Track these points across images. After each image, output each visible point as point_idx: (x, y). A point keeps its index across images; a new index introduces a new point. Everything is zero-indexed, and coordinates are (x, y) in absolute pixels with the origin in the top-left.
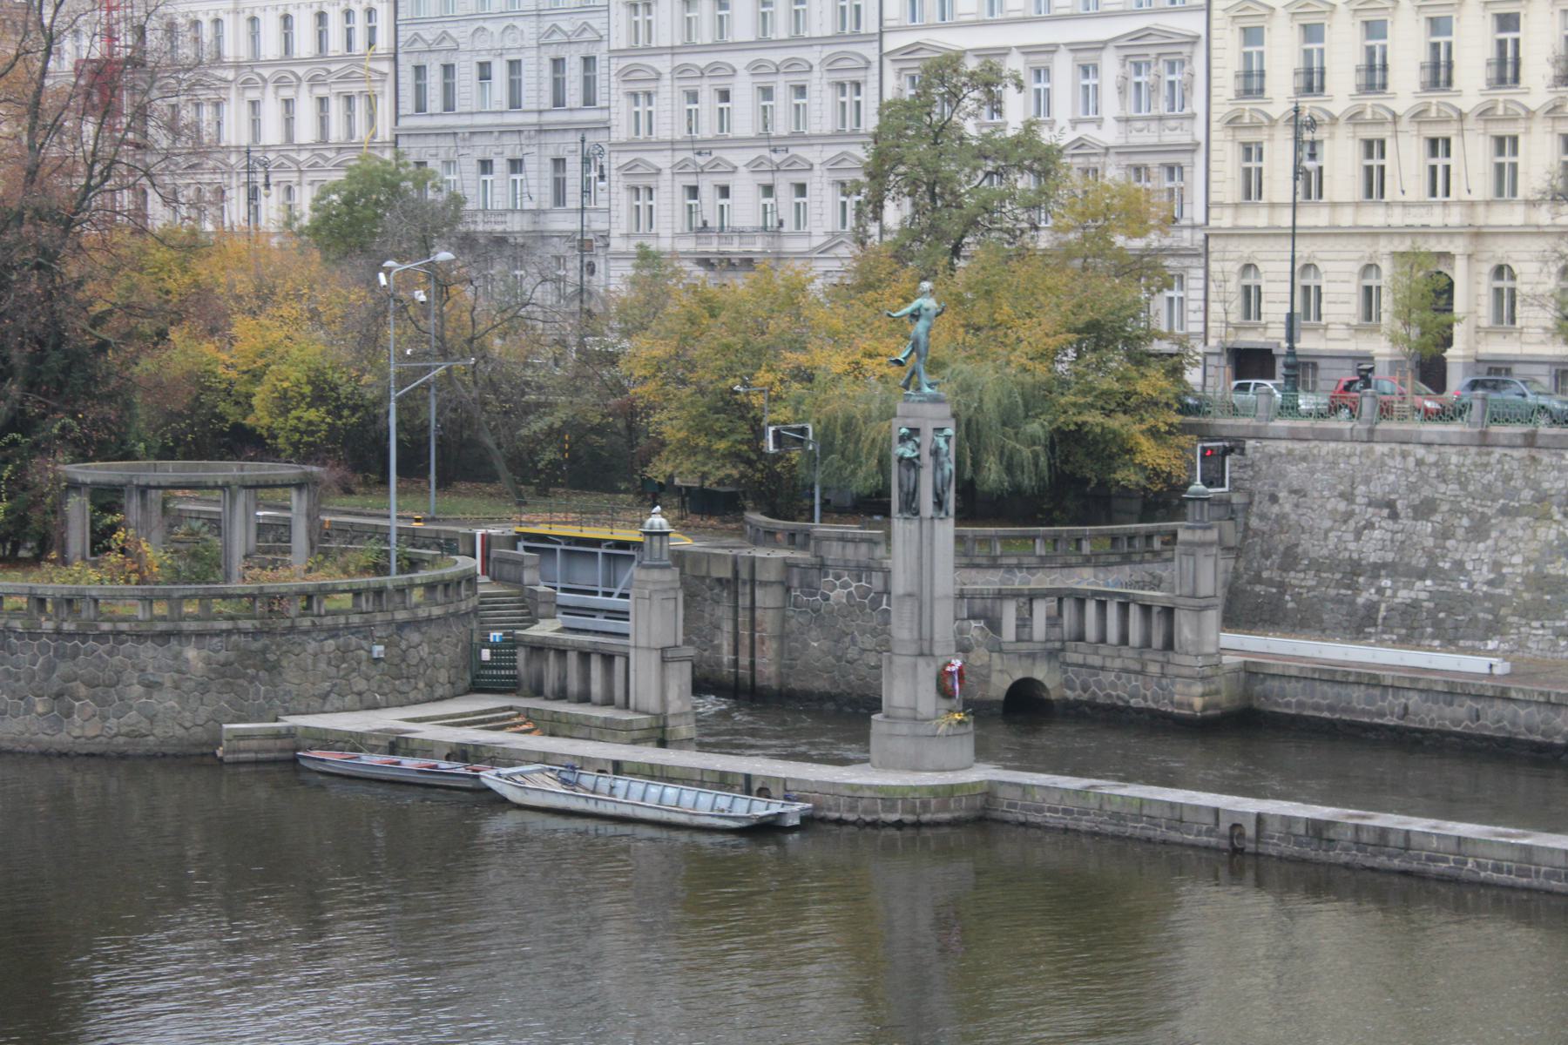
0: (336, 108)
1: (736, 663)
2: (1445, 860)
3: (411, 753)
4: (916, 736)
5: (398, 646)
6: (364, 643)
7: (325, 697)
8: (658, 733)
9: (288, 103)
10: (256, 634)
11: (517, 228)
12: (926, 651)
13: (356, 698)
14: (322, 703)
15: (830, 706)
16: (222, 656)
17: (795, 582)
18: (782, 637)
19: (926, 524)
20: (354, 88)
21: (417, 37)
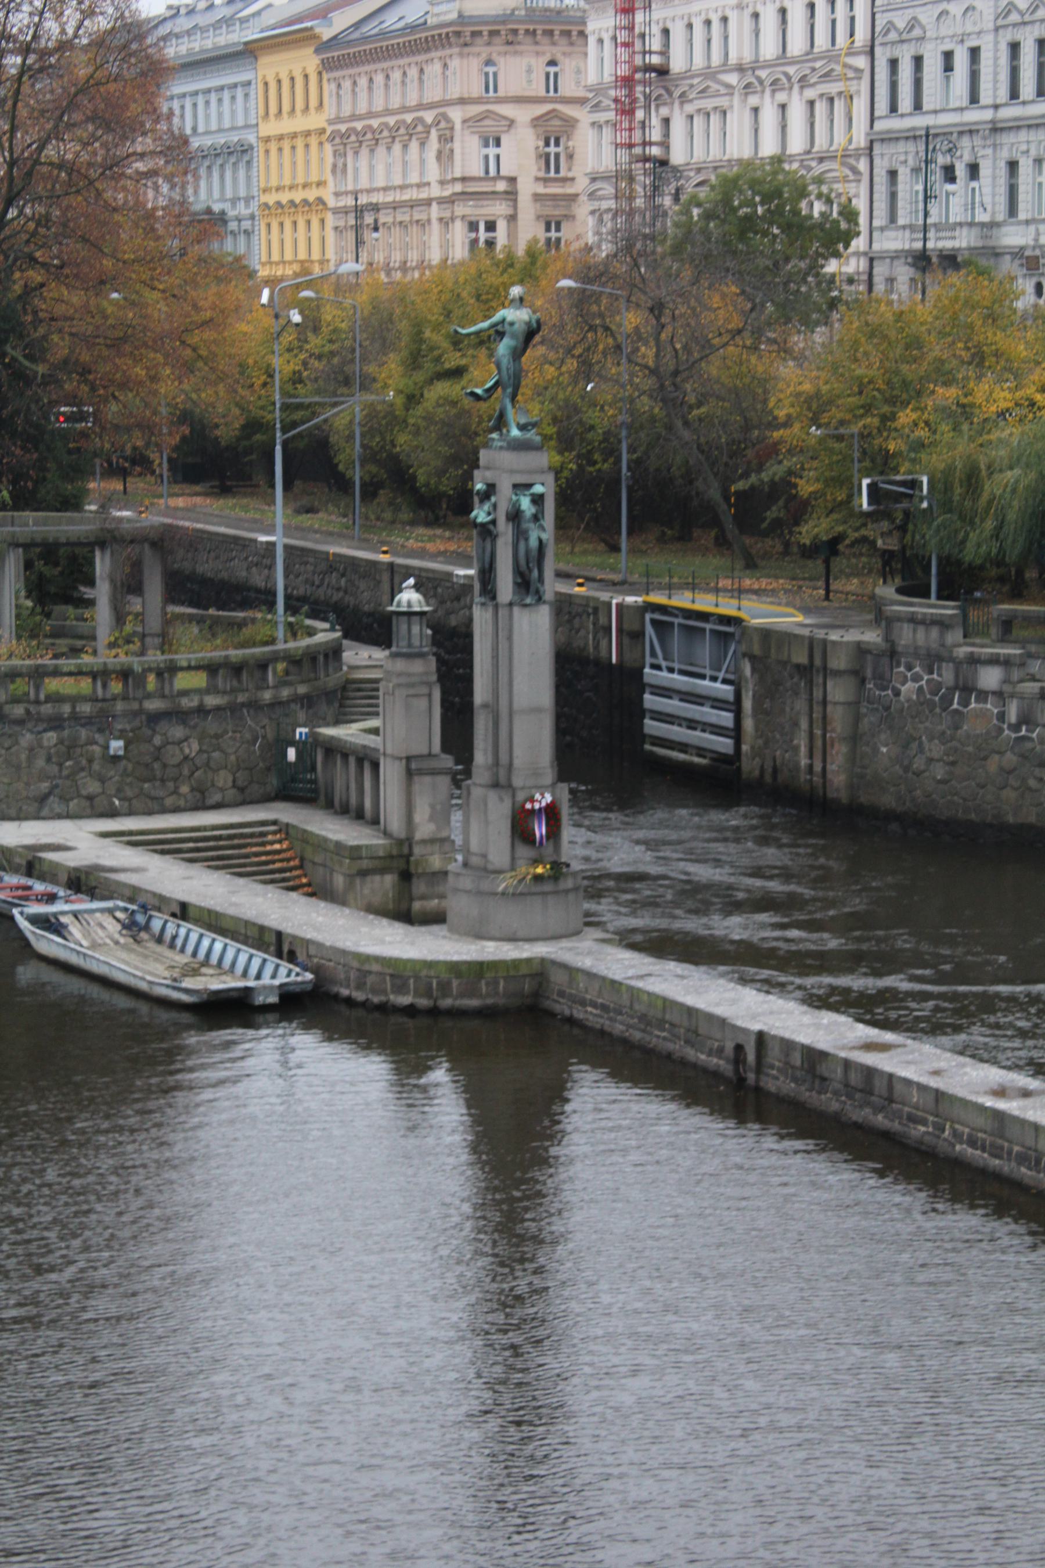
1: (811, 767)
3: (42, 878)
7: (43, 799)
9: (783, 107)
11: (964, 245)
12: (503, 780)
13: (86, 803)
15: (894, 827)
17: (869, 673)
18: (854, 738)
19: (502, 612)
20: (833, 88)
21: (890, 26)
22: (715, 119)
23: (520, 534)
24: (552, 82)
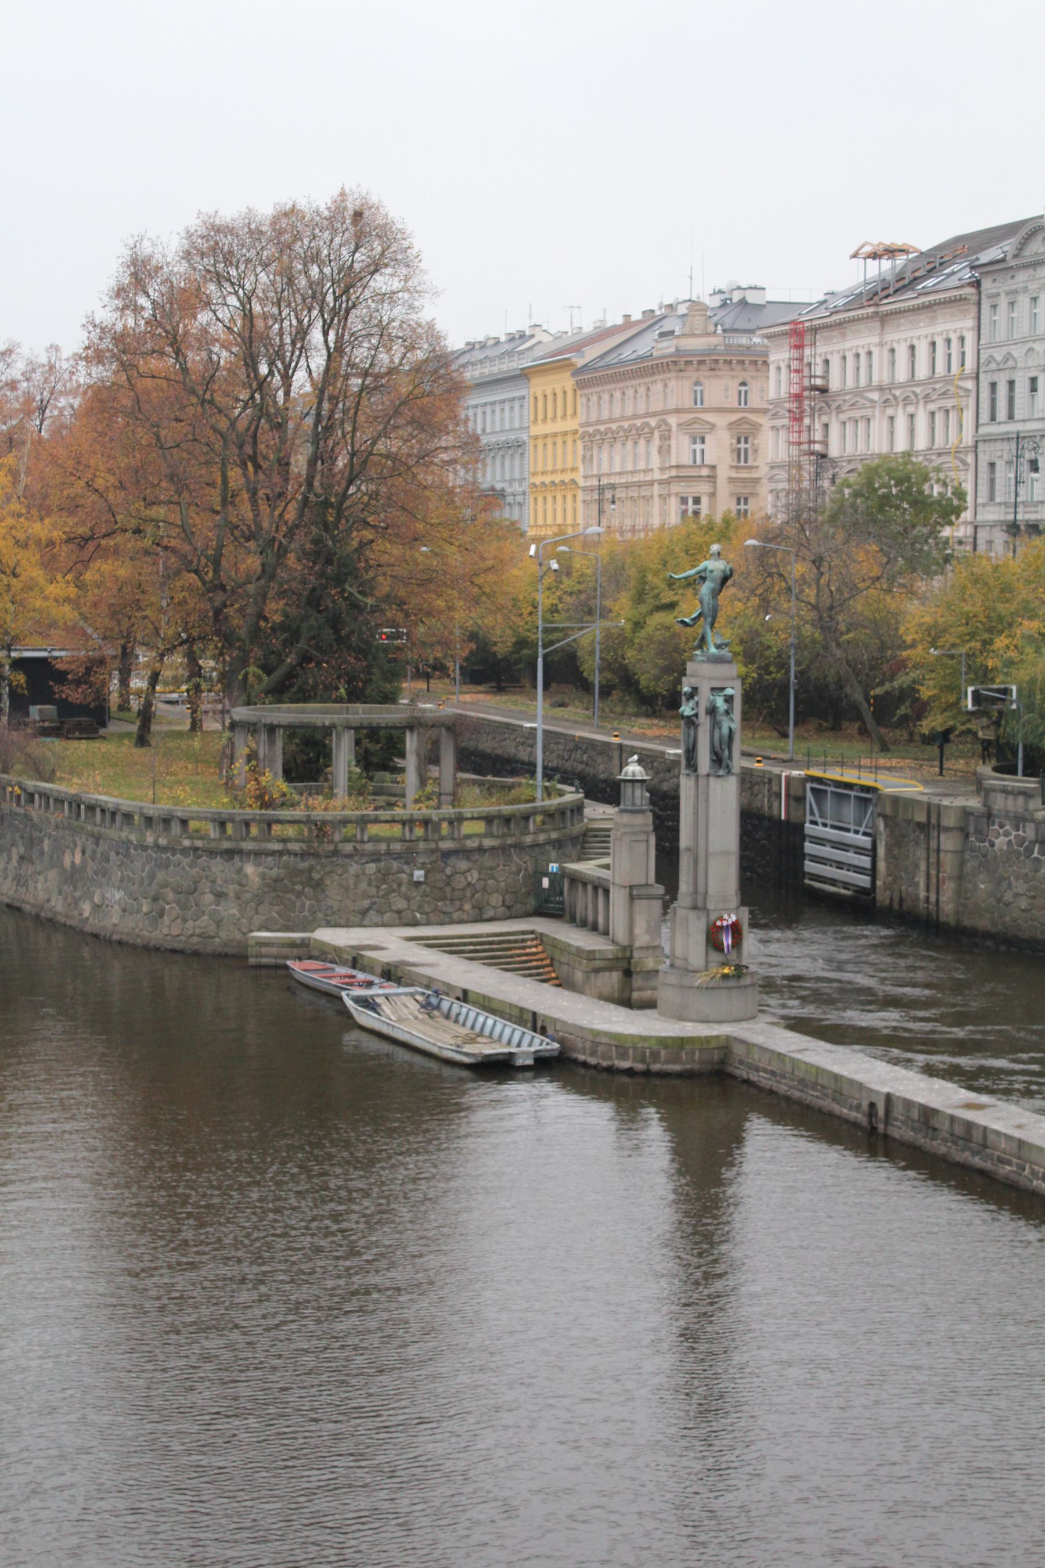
0: (939, 418)
2: (1009, 1163)
4: (682, 987)
5: (443, 871)
6: (406, 868)
7: (364, 912)
8: (625, 964)
9: (912, 416)
10: (303, 855)
12: (700, 904)
13: (396, 916)
14: (361, 919)
16: (274, 873)
17: (971, 829)
18: (960, 877)
22: (861, 425)
23: (715, 724)
24: (743, 397)
